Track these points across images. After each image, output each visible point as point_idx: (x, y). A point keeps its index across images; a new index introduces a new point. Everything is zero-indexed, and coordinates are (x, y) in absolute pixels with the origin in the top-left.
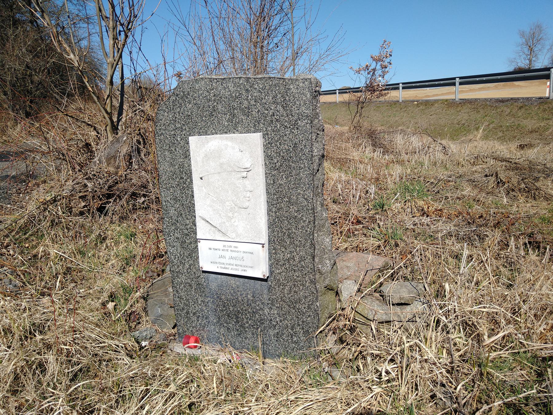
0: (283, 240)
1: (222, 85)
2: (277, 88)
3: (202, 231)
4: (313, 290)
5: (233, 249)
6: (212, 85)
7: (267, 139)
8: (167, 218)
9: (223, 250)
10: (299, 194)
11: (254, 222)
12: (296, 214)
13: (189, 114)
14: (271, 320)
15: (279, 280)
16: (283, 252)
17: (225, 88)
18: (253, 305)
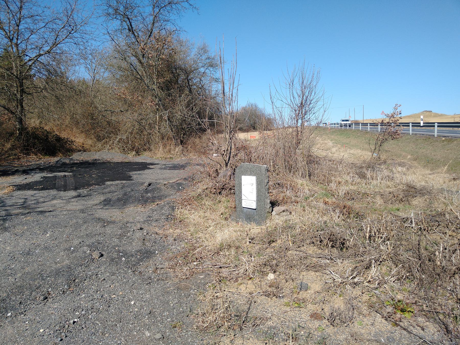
3: (243, 197)
11: (253, 196)
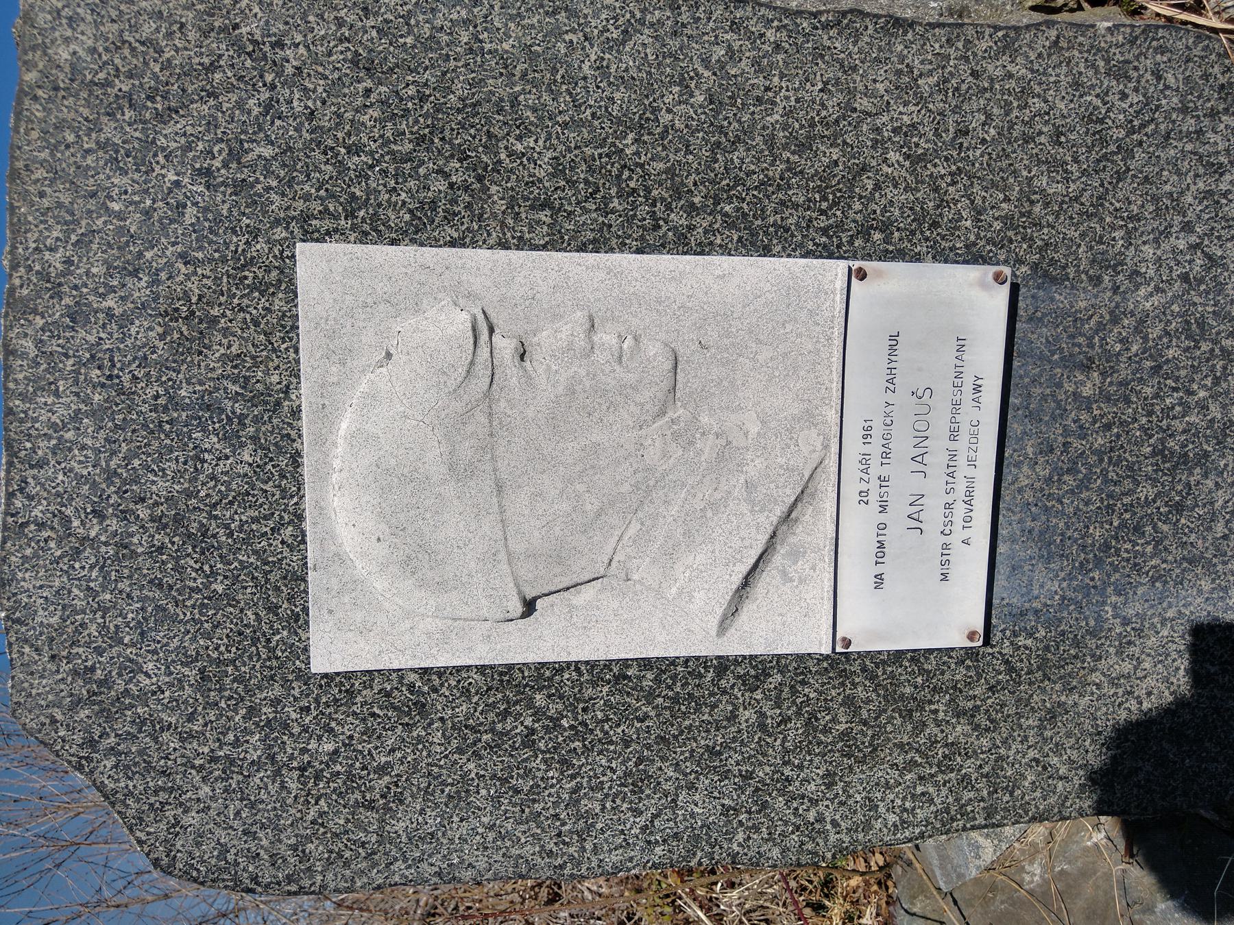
0: (824, 177)
1: (41, 464)
2: (71, 138)
4: (1042, 43)
5: (876, 449)
6: (41, 526)
7: (327, 224)
8: (730, 835)
9: (883, 509)
10: (601, 68)
12: (700, 98)
13: (192, 673)
14: (1185, 278)
15: (1007, 220)
16: (877, 187)
17: (62, 448)
18: (1124, 372)
